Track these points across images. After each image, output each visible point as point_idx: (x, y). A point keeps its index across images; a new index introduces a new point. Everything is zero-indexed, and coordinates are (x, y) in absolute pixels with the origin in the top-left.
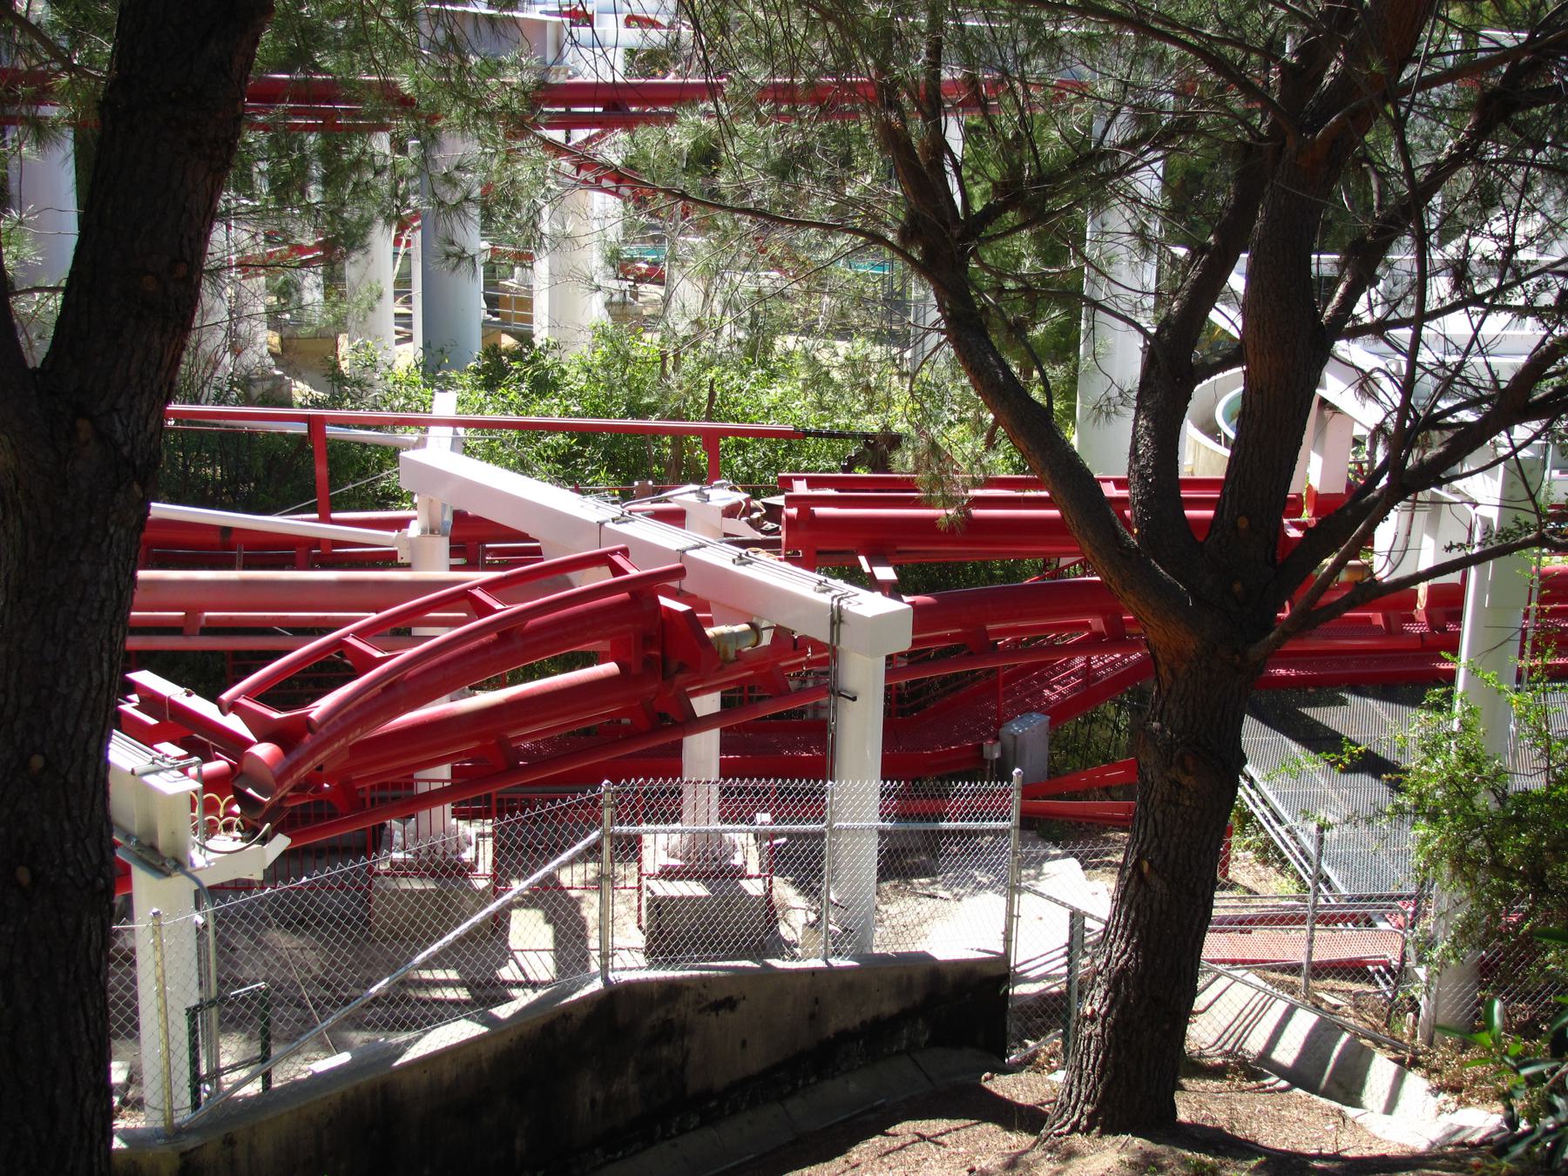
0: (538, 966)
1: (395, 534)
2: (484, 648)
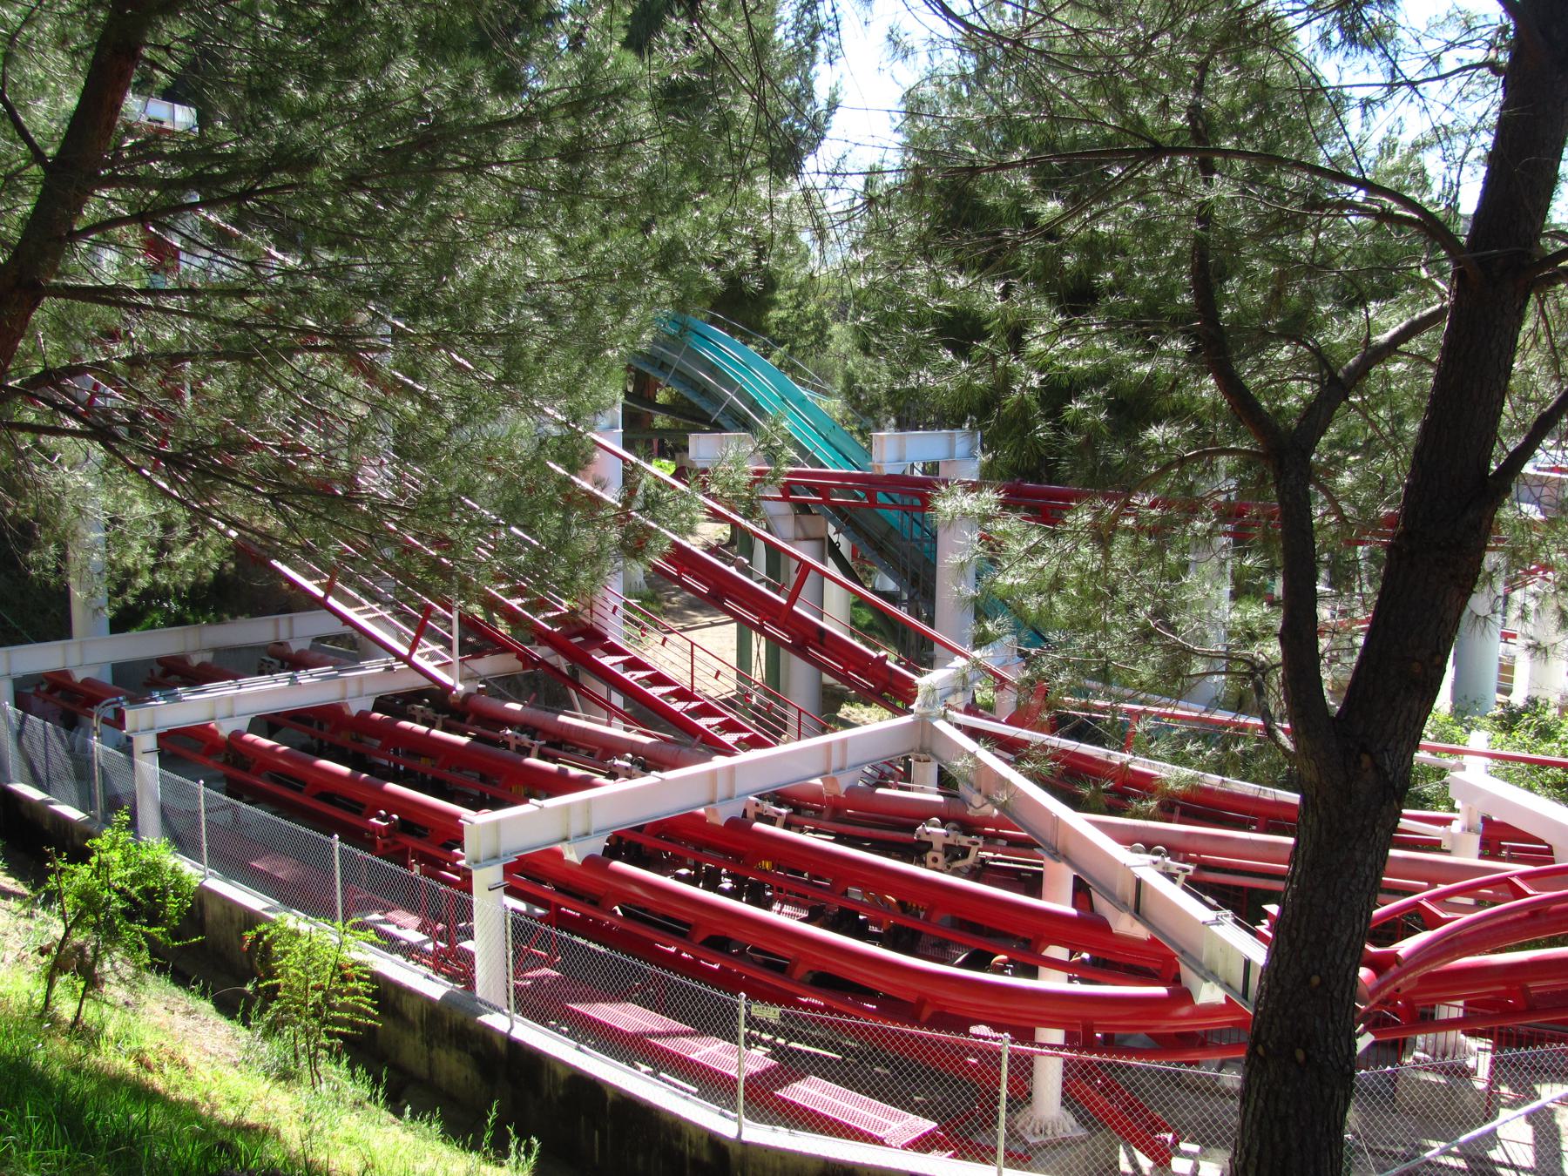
0: (1521, 1156)
1: (1441, 829)
2: (1518, 920)
